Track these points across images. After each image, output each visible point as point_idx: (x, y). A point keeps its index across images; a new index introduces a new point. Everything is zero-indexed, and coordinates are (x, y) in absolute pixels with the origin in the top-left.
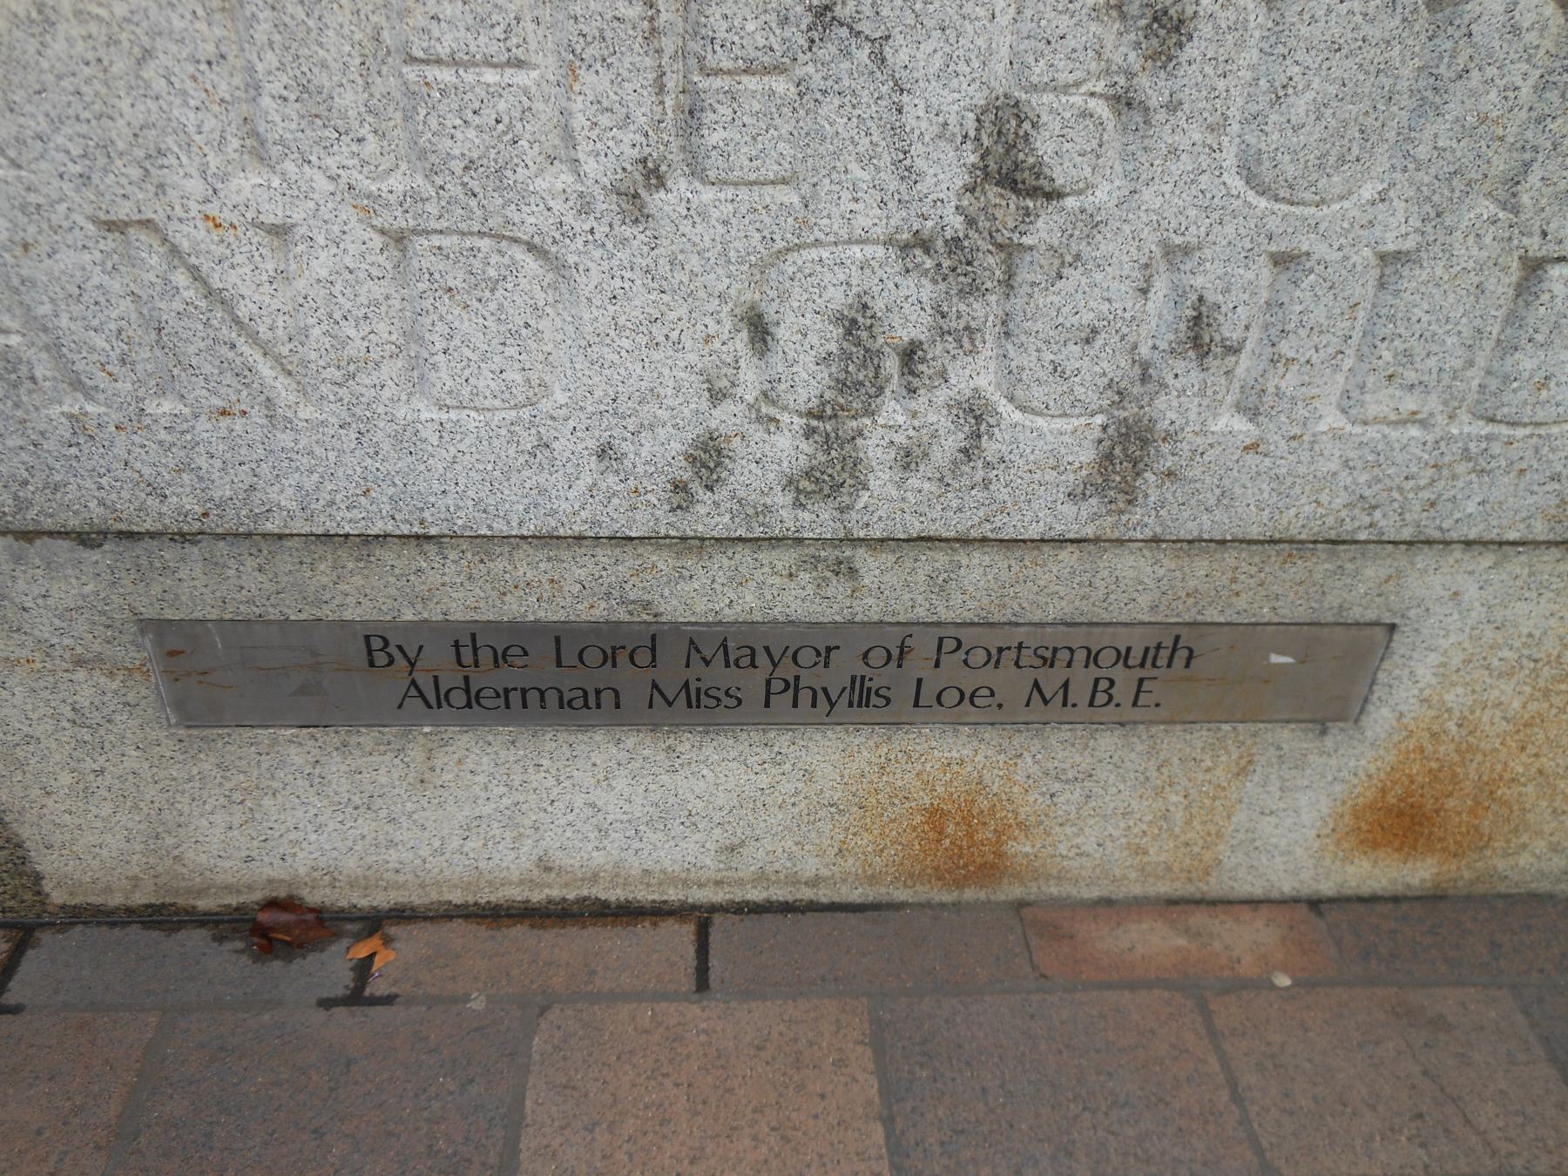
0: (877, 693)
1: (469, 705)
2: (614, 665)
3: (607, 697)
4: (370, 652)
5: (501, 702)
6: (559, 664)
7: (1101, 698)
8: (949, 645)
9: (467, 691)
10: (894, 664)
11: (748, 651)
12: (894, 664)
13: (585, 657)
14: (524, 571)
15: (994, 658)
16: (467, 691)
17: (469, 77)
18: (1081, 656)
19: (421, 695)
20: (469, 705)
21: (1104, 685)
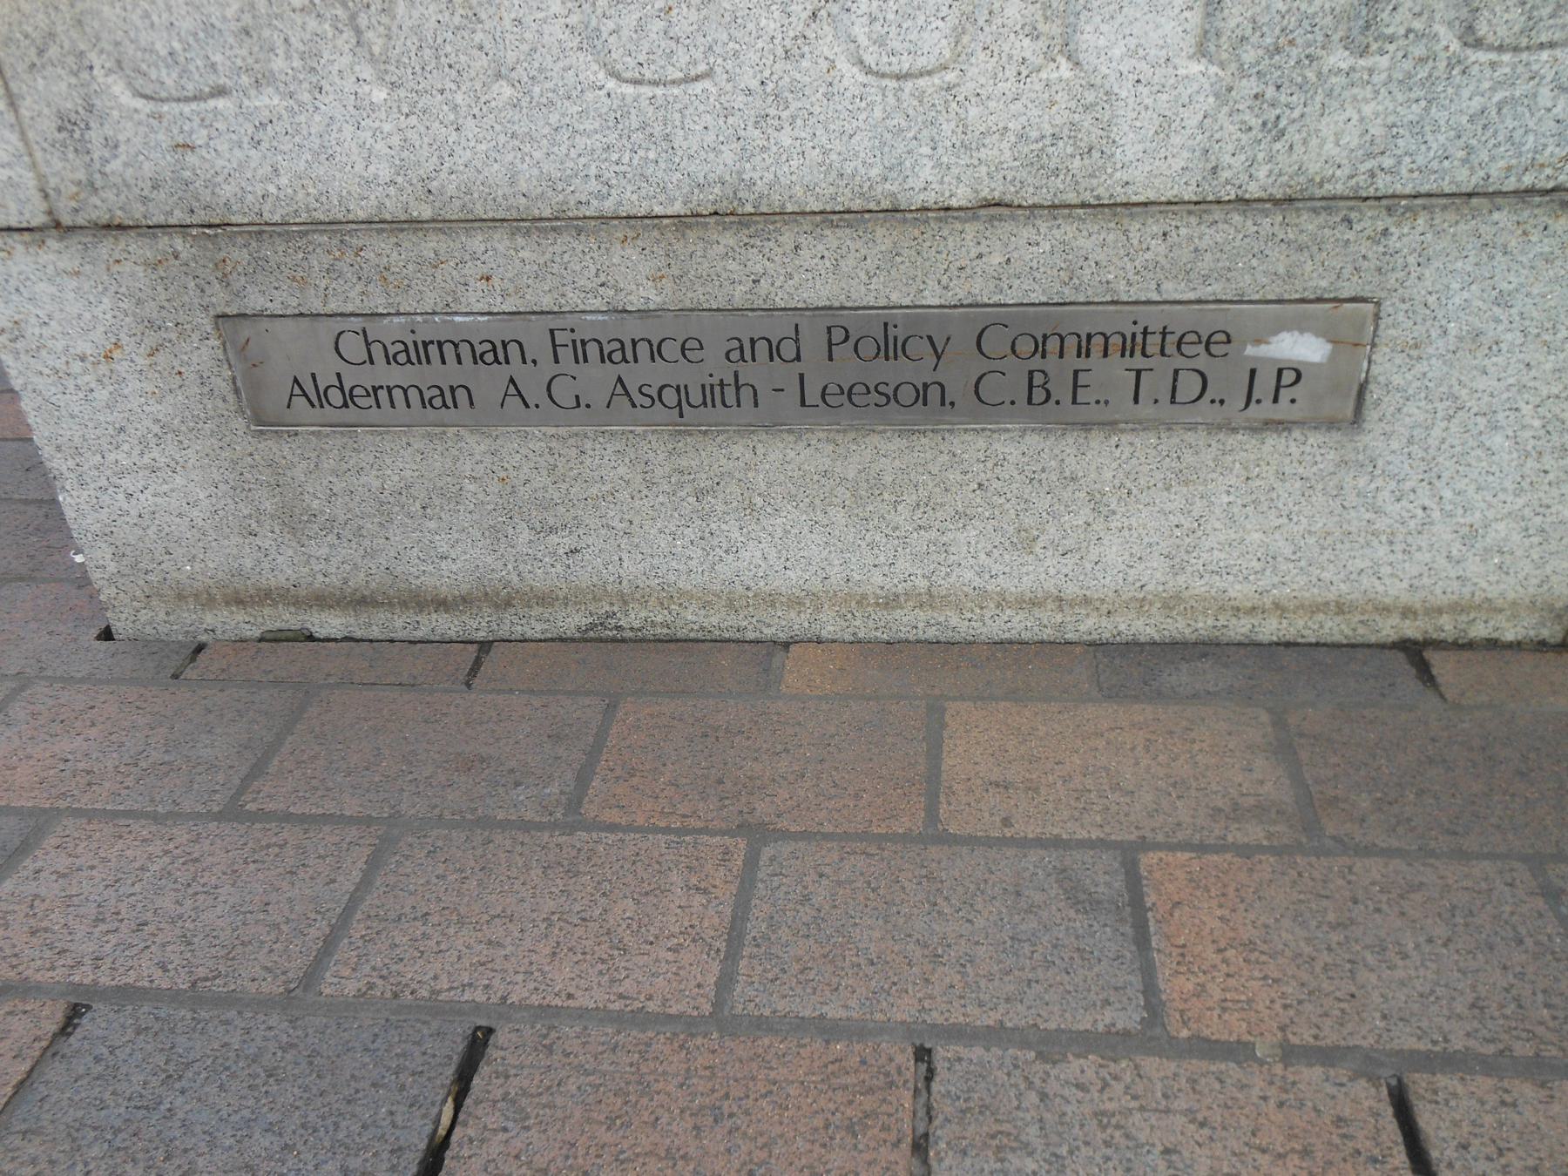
0: (887, 396)
1: (345, 405)
2: (925, 404)
3: (461, 395)
4: (1031, 387)
5: (371, 401)
6: (803, 403)
7: (1039, 395)
8: (838, 335)
9: (342, 389)
10: (1038, 355)
11: (618, 345)
12: (1038, 355)
13: (1017, 348)
14: (539, 627)
15: (744, 350)
16: (342, 389)
17: (165, 108)
18: (1071, 343)
19: (305, 395)
20: (345, 405)
21: (1038, 379)
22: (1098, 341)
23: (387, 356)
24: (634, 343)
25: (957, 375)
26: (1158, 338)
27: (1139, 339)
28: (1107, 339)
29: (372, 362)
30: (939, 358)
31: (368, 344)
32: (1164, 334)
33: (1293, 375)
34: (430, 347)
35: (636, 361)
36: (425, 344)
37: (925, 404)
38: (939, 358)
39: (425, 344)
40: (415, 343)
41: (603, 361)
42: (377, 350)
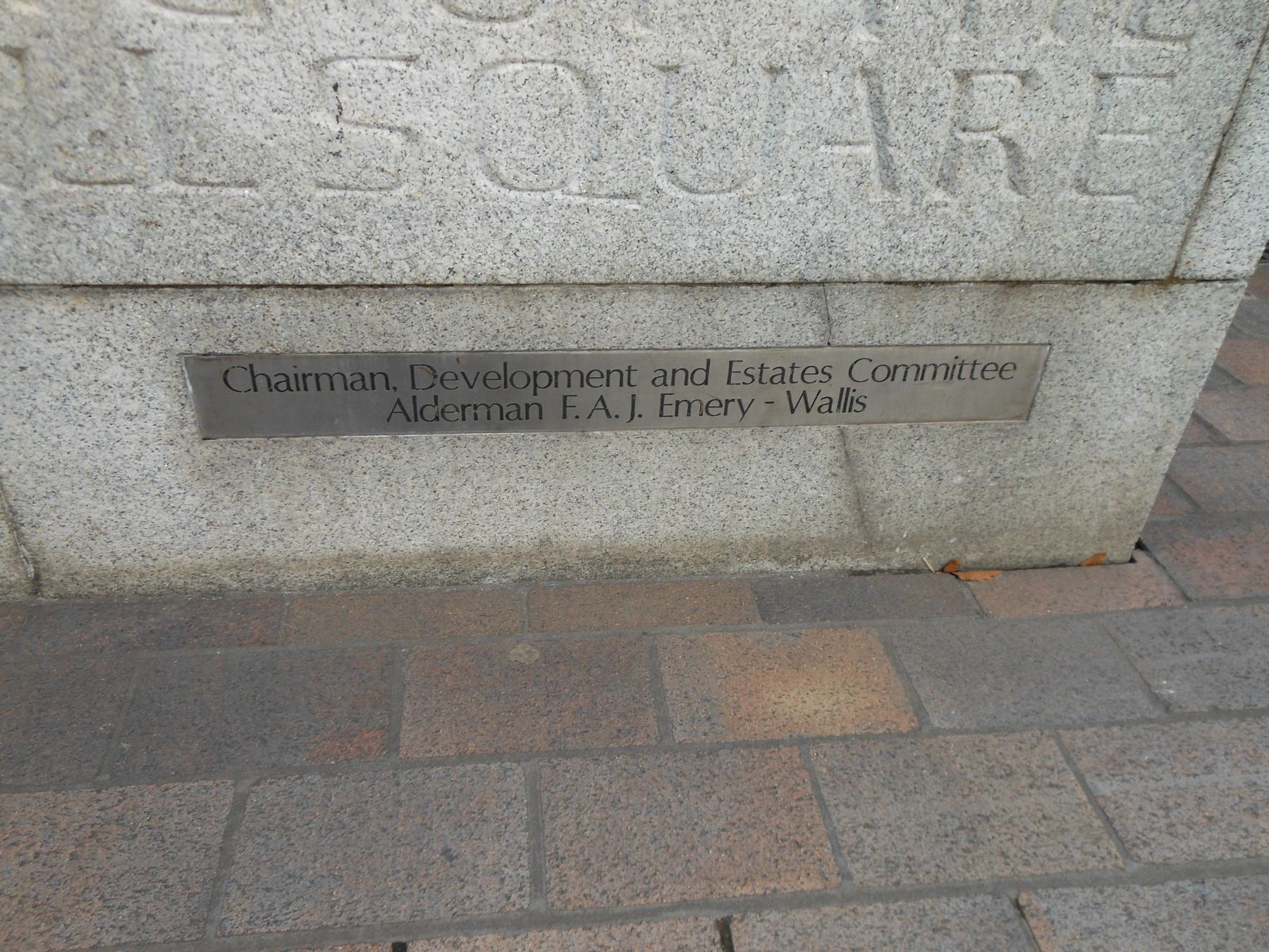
2: (556, 386)
22: (930, 371)
23: (269, 385)
24: (372, 375)
25: (617, 397)
26: (970, 367)
27: (958, 367)
28: (331, 377)
29: (256, 390)
30: (744, 413)
31: (254, 377)
32: (975, 364)
33: (657, 382)
34: (308, 379)
35: (373, 388)
36: (304, 376)
37: (556, 386)
38: (744, 413)
39: (304, 376)
40: (296, 376)
41: (346, 389)
42: (261, 381)
